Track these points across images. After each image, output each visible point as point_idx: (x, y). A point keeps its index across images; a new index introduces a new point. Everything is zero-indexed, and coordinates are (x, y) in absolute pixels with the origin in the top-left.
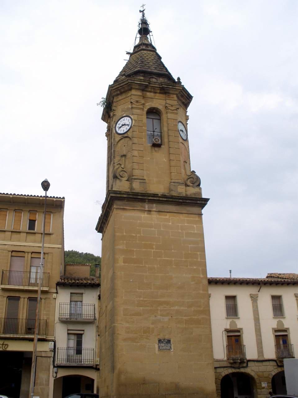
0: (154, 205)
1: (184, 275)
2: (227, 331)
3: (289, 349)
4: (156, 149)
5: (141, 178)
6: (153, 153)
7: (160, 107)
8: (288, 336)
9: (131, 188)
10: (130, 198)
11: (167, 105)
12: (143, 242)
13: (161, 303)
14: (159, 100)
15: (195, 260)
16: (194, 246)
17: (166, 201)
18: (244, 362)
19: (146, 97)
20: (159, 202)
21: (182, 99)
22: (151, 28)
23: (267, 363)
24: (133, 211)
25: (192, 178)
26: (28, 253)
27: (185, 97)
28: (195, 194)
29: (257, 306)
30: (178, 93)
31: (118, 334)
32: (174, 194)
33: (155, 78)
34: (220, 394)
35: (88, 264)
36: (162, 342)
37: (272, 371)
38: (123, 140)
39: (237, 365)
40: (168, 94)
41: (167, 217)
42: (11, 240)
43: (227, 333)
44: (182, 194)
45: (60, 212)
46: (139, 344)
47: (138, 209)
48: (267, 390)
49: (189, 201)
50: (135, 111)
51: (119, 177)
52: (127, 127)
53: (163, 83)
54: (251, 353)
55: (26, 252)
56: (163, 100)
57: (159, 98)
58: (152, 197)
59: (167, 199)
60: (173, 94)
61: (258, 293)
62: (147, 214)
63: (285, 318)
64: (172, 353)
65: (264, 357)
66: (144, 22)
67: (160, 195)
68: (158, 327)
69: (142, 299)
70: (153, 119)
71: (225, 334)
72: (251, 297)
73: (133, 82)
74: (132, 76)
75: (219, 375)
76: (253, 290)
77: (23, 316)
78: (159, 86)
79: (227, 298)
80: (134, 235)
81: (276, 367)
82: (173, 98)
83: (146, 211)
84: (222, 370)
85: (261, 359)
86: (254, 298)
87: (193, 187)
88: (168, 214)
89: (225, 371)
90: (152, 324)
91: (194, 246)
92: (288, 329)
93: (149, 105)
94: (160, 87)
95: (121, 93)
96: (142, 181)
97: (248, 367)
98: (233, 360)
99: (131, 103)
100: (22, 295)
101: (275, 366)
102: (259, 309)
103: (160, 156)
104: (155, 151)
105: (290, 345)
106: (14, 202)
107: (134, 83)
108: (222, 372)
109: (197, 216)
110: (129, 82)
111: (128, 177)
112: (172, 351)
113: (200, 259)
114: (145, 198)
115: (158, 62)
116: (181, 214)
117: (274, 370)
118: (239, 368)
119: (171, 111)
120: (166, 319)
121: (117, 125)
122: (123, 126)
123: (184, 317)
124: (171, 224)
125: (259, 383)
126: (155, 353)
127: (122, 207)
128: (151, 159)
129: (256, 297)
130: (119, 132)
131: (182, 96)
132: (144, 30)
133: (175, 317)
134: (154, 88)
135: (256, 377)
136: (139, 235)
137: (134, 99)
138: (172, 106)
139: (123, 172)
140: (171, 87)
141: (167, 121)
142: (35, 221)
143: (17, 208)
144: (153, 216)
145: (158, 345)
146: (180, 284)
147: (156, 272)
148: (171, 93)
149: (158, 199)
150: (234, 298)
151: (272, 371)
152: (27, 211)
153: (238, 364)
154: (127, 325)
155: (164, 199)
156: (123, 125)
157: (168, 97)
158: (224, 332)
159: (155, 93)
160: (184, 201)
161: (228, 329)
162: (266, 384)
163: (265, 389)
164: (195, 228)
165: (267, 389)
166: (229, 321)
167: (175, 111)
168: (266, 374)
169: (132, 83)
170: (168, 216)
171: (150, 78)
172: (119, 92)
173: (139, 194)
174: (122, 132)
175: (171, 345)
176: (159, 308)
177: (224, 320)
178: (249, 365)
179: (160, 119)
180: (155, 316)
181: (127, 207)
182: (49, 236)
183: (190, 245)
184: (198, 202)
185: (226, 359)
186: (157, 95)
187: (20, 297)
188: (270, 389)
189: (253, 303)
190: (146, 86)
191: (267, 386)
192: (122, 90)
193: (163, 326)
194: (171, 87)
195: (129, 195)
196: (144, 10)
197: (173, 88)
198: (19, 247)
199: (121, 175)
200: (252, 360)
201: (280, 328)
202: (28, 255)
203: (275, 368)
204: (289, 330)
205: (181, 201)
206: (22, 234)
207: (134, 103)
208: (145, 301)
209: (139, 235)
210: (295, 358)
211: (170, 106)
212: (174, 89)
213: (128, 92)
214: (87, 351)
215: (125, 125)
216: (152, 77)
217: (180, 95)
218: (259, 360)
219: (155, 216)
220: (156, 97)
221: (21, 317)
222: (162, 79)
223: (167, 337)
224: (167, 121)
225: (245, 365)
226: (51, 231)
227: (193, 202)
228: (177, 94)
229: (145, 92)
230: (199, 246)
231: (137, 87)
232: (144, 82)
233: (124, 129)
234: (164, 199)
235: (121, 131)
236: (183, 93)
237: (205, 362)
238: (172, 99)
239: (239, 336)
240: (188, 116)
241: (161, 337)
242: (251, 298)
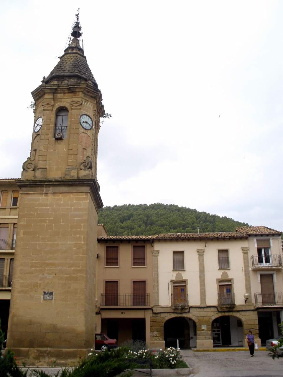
0: (51, 188)
1: (69, 242)
2: (173, 282)
3: (232, 297)
4: (59, 142)
5: (43, 168)
6: (56, 146)
7: (67, 105)
8: (232, 285)
9: (35, 177)
11: (72, 103)
12: (39, 218)
13: (48, 265)
15: (79, 230)
16: (80, 218)
17: (59, 184)
18: (185, 308)
19: (58, 98)
20: (54, 186)
21: (89, 94)
22: (82, 31)
23: (209, 309)
24: (34, 194)
26: (11, 224)
27: (91, 92)
28: (85, 176)
29: (203, 260)
30: (83, 90)
31: (15, 288)
32: (68, 178)
33: (67, 80)
34: (163, 334)
35: (100, 224)
36: (47, 294)
37: (213, 316)
39: (179, 311)
40: (74, 93)
41: (60, 197)
43: (173, 283)
44: (73, 177)
46: (29, 295)
47: (38, 192)
48: (206, 331)
49: (77, 183)
53: (69, 85)
54: (194, 299)
55: (10, 224)
58: (47, 182)
59: (60, 183)
60: (79, 92)
61: (205, 248)
62: (45, 196)
63: (185, 270)
64: (53, 302)
65: (207, 304)
67: (53, 181)
68: (44, 283)
69: (34, 261)
70: (63, 115)
71: (171, 285)
72: (198, 252)
73: (45, 88)
75: (163, 319)
76: (200, 246)
77: (6, 273)
78: (66, 87)
79: (220, 251)
80: (33, 213)
81: (217, 312)
82: (79, 95)
84: (166, 314)
85: (203, 305)
86: (201, 253)
88: (61, 194)
89: (168, 316)
90: (40, 280)
91: (80, 218)
92: (232, 279)
93: (57, 105)
94: (67, 88)
96: (44, 170)
97: (190, 313)
98: (175, 306)
100: (6, 257)
101: (215, 311)
102: (205, 262)
103: (62, 147)
104: (58, 143)
105: (233, 293)
106: (12, 185)
107: (46, 89)
108: (166, 317)
110: (42, 89)
111: (33, 168)
112: (53, 301)
113: (83, 229)
114: (43, 183)
115: (81, 62)
116: (71, 194)
117: (215, 315)
118: (181, 313)
120: (51, 276)
123: (65, 275)
124: (62, 202)
125: (199, 326)
126: (40, 302)
127: (26, 192)
128: (53, 150)
129: (203, 251)
131: (88, 92)
132: (76, 33)
133: (58, 275)
135: (196, 321)
136: (37, 213)
138: (77, 103)
139: (29, 164)
142: (18, 198)
143: (3, 190)
144: (49, 197)
145: (43, 296)
146: (64, 249)
147: (47, 240)
148: (77, 92)
149: (52, 183)
150: (226, 251)
151: (213, 316)
152: (11, 191)
153: (180, 310)
154: (22, 281)
155: (57, 183)
157: (74, 95)
158: (170, 283)
159: (65, 93)
160: (73, 183)
161: (174, 280)
162: (206, 327)
163: (205, 331)
164: (81, 204)
165: (207, 331)
166: (175, 274)
167: (79, 106)
168: (206, 319)
169: (44, 89)
170: (60, 196)
172: (38, 97)
173: (38, 181)
175: (53, 296)
176: (46, 268)
177: (170, 272)
178: (190, 311)
180: (43, 274)
181: (29, 192)
183: (75, 218)
184: (85, 183)
185: (170, 305)
186: (67, 94)
187: (4, 258)
188: (210, 331)
189: (199, 257)
190: (56, 89)
191: (206, 328)
192: (40, 96)
193: (48, 282)
195: (30, 182)
196: (78, 14)
197: (78, 87)
198: (4, 220)
199: (28, 167)
200: (194, 306)
201: (224, 279)
202: (11, 226)
203: (215, 313)
204: (233, 280)
205: (71, 183)
206: (7, 210)
207: (45, 105)
208: (37, 263)
209: (37, 213)
211: (75, 103)
212: (79, 88)
214: (123, 297)
216: (64, 79)
217: (86, 91)
218: (201, 306)
219: (50, 197)
220: (65, 97)
221: (5, 274)
222: (73, 80)
223: (50, 290)
225: (187, 311)
227: (81, 183)
228: (82, 92)
230: (84, 218)
231: (49, 92)
232: (54, 86)
234: (57, 183)
236: (88, 89)
237: (79, 309)
238: (79, 96)
239: (185, 286)
241: (46, 290)
242: (198, 253)
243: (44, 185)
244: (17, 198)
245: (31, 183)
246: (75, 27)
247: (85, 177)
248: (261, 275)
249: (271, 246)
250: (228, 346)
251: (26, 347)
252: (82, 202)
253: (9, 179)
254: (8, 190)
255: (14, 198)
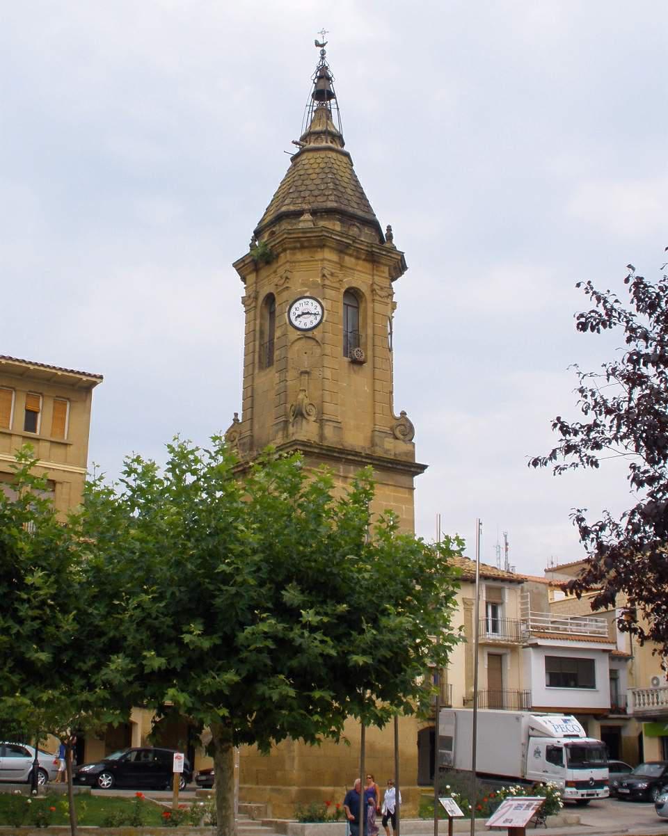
4: (356, 367)
7: (364, 289)
10: (323, 454)
11: (376, 287)
14: (362, 274)
22: (336, 87)
25: (403, 425)
33: (357, 227)
38: (303, 341)
42: (9, 452)
45: (85, 401)
50: (329, 292)
51: (306, 415)
52: (312, 317)
56: (369, 274)
57: (364, 271)
58: (353, 455)
60: (386, 265)
62: (342, 481)
66: (323, 76)
67: (363, 454)
73: (330, 235)
74: (319, 214)
78: (366, 248)
82: (384, 272)
83: (340, 476)
87: (404, 441)
94: (367, 251)
95: (303, 247)
96: (339, 427)
99: (324, 276)
104: (355, 371)
107: (331, 237)
109: (407, 490)
119: (380, 299)
121: (293, 310)
122: (304, 316)
130: (296, 323)
132: (323, 94)
134: (358, 251)
137: (329, 268)
138: (382, 289)
140: (384, 253)
141: (373, 316)
148: (382, 264)
149: (360, 459)
156: (303, 314)
157: (377, 271)
160: (395, 466)
169: (328, 237)
171: (351, 225)
173: (337, 450)
174: (302, 326)
179: (358, 308)
182: (63, 447)
190: (348, 246)
194: (384, 253)
195: (321, 449)
205: (390, 465)
207: (328, 276)
210: (450, 707)
213: (315, 249)
215: (308, 313)
220: (359, 268)
224: (373, 316)
226: (65, 440)
229: (342, 255)
231: (333, 246)
233: (305, 321)
235: (301, 323)
240: (395, 303)
243: (344, 460)
244: (36, 413)
245: (324, 452)
246: (319, 78)
247: (407, 456)
248: (490, 655)
249: (506, 601)
250: (163, 788)
251: (328, 786)
252: (404, 506)
253: (36, 364)
254: (45, 393)
255: (28, 411)
